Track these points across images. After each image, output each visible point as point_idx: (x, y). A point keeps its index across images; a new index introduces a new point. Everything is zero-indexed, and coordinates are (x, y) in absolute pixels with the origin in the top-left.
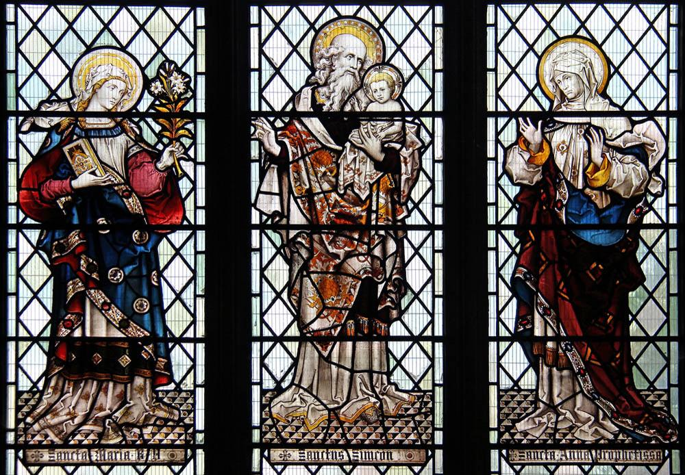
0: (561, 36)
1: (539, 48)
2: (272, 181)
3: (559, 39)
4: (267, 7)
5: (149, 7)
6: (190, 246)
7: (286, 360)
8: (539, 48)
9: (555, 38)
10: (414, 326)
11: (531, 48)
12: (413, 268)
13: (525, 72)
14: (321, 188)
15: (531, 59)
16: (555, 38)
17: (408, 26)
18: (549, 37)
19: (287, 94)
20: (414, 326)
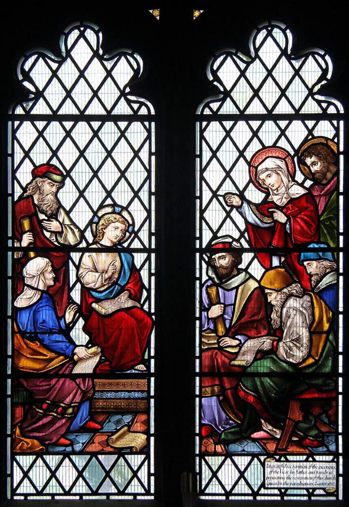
0: (267, 145)
1: (249, 155)
2: (325, 281)
3: (264, 147)
4: (51, 113)
5: (142, 114)
6: (145, 468)
7: (142, 173)
8: (249, 155)
9: (261, 147)
10: (93, 161)
11: (242, 154)
12: (274, 133)
13: (41, 468)
14: (98, 391)
15: (242, 165)
16: (261, 147)
17: (116, 134)
18: (255, 146)
19: (47, 75)
20: (93, 161)
